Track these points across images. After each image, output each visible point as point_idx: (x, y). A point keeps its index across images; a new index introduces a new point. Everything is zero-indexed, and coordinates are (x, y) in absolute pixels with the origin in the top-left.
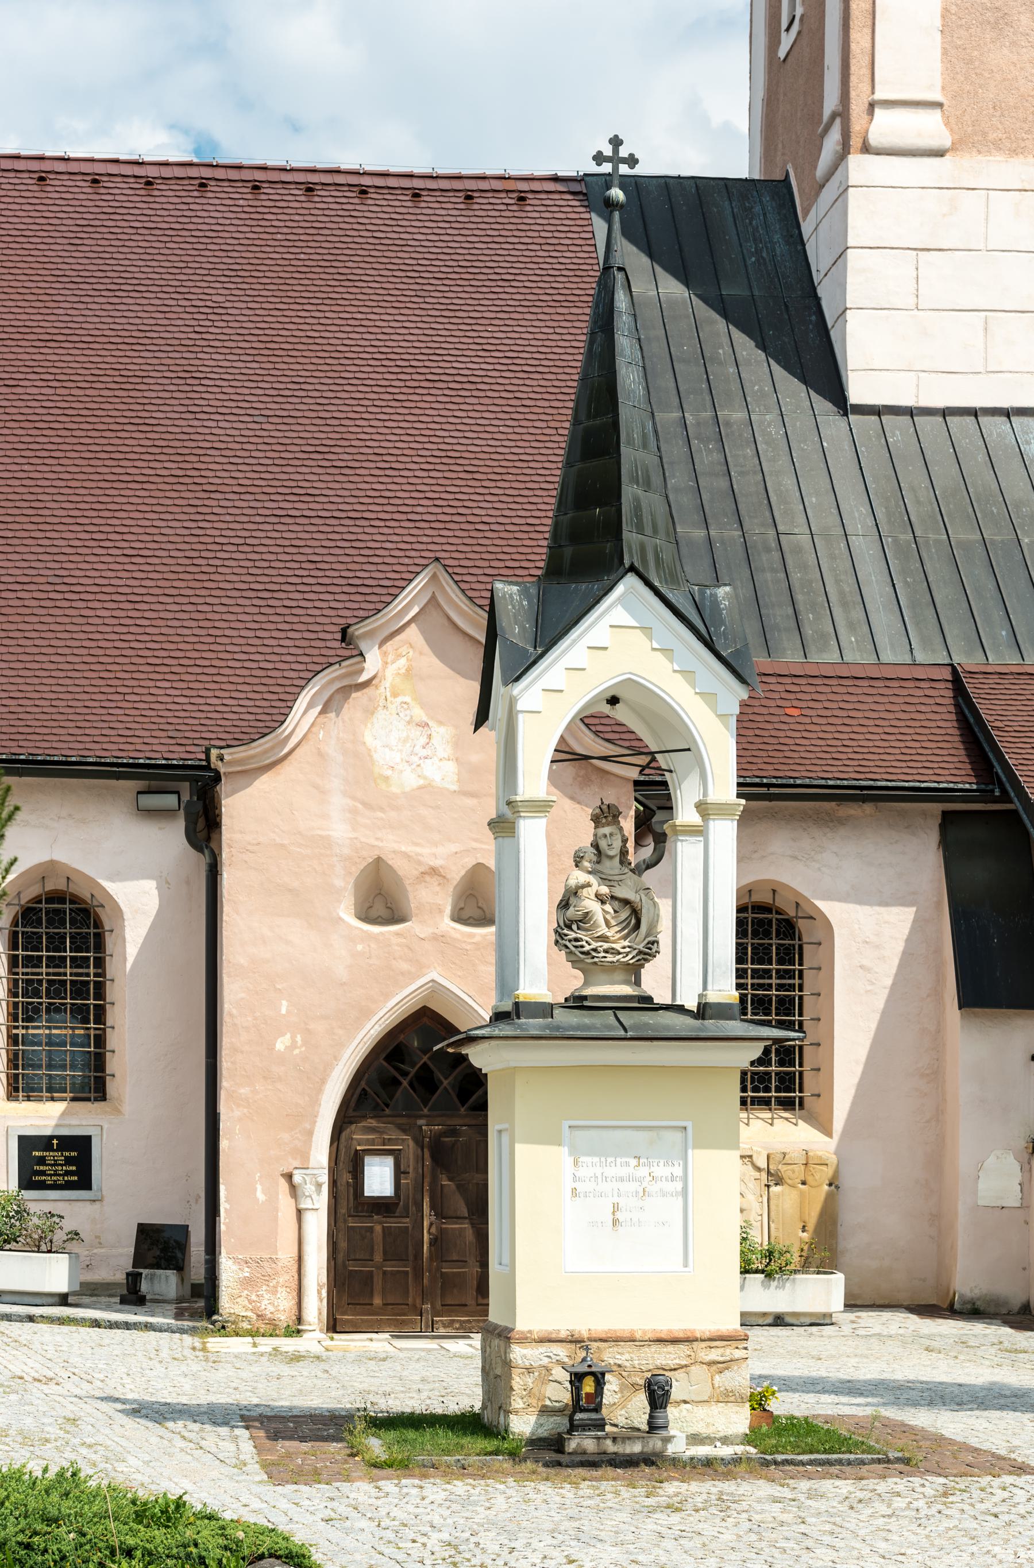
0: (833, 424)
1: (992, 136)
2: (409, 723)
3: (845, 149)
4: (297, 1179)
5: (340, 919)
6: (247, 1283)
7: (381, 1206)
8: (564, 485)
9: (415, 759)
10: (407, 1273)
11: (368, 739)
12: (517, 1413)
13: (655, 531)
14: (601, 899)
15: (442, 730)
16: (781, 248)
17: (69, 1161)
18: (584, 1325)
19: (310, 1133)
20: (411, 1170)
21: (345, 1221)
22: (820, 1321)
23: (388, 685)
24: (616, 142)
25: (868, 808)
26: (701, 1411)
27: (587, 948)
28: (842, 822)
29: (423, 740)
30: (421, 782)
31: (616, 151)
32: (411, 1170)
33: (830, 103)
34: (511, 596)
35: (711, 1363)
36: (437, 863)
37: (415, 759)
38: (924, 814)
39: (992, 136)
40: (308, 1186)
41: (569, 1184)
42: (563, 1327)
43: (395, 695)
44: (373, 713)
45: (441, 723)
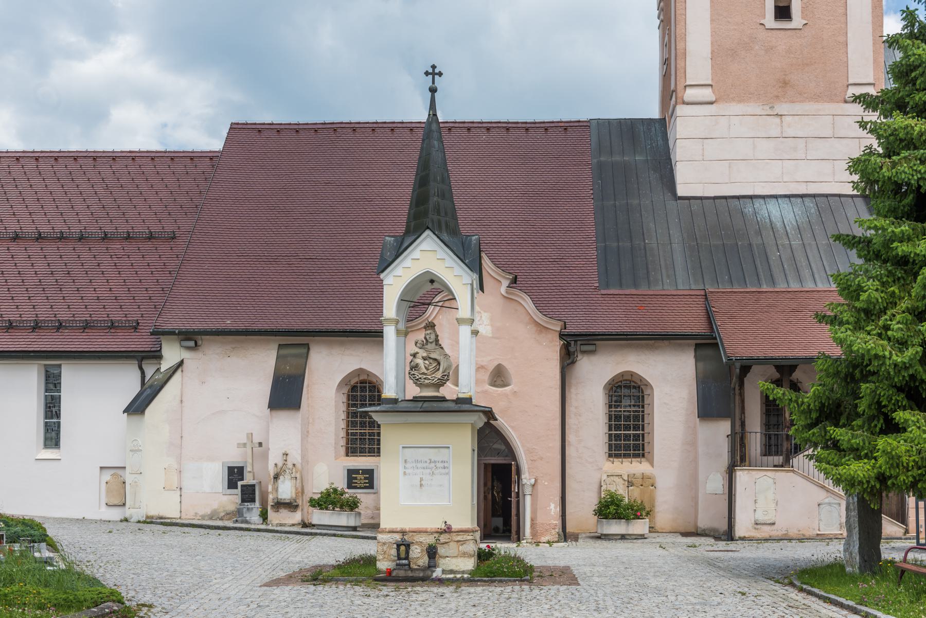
0: (671, 204)
1: (731, 96)
3: (676, 103)
8: (412, 199)
13: (446, 214)
14: (424, 359)
16: (660, 142)
17: (365, 478)
18: (407, 526)
22: (642, 537)
24: (434, 67)
25: (666, 342)
26: (454, 561)
28: (657, 348)
31: (434, 70)
33: (672, 87)
35: (458, 541)
36: (483, 364)
38: (689, 345)
39: (731, 96)
42: (398, 526)
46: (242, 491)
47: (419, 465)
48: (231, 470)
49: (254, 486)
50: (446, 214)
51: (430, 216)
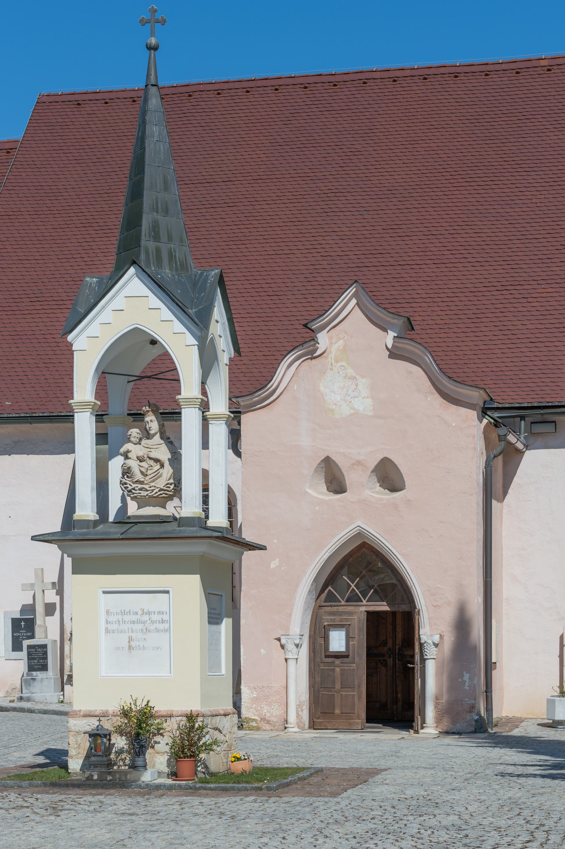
2: (345, 377)
4: (283, 641)
5: (307, 492)
6: (256, 700)
7: (338, 656)
9: (348, 398)
10: (354, 695)
11: (322, 388)
12: (72, 757)
13: (170, 239)
15: (364, 380)
19: (290, 615)
20: (356, 636)
21: (319, 666)
23: (333, 356)
27: (130, 488)
29: (353, 387)
30: (352, 411)
32: (356, 636)
34: (91, 284)
37: (348, 398)
40: (289, 645)
41: (103, 625)
43: (337, 362)
44: (324, 373)
45: (363, 377)
46: (29, 654)
47: (127, 618)
48: (16, 623)
49: (45, 646)
50: (170, 239)
51: (143, 243)
